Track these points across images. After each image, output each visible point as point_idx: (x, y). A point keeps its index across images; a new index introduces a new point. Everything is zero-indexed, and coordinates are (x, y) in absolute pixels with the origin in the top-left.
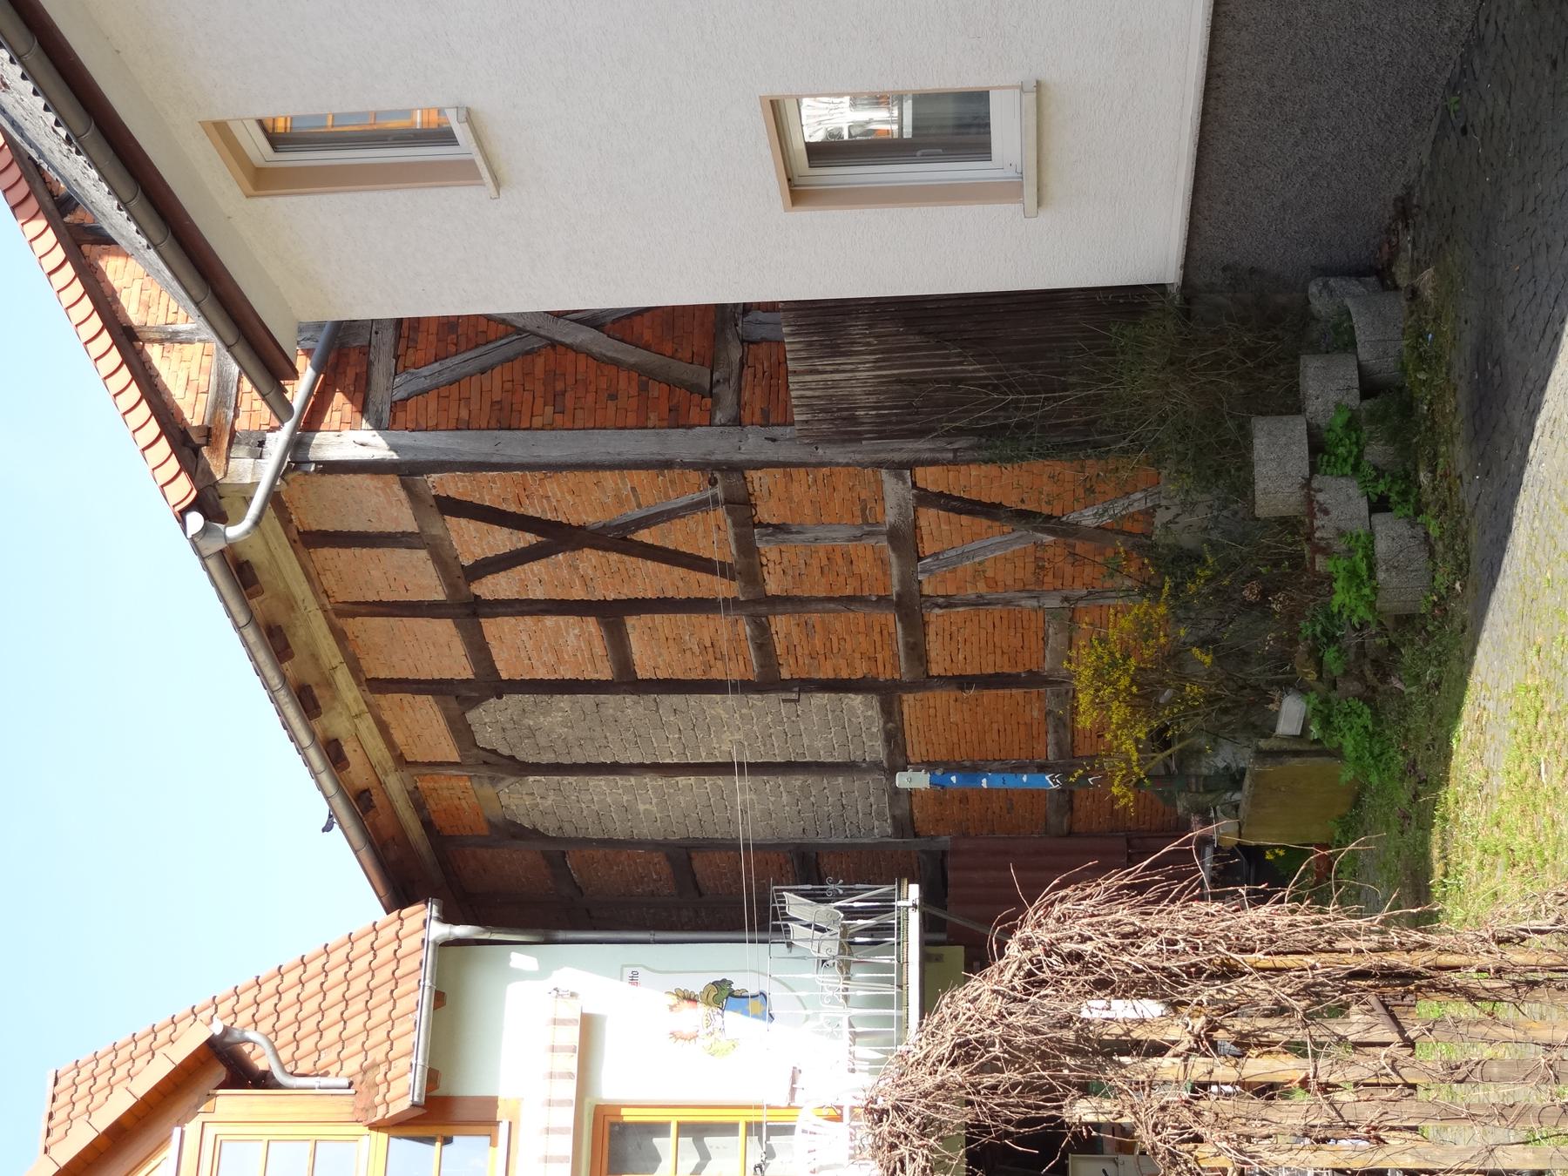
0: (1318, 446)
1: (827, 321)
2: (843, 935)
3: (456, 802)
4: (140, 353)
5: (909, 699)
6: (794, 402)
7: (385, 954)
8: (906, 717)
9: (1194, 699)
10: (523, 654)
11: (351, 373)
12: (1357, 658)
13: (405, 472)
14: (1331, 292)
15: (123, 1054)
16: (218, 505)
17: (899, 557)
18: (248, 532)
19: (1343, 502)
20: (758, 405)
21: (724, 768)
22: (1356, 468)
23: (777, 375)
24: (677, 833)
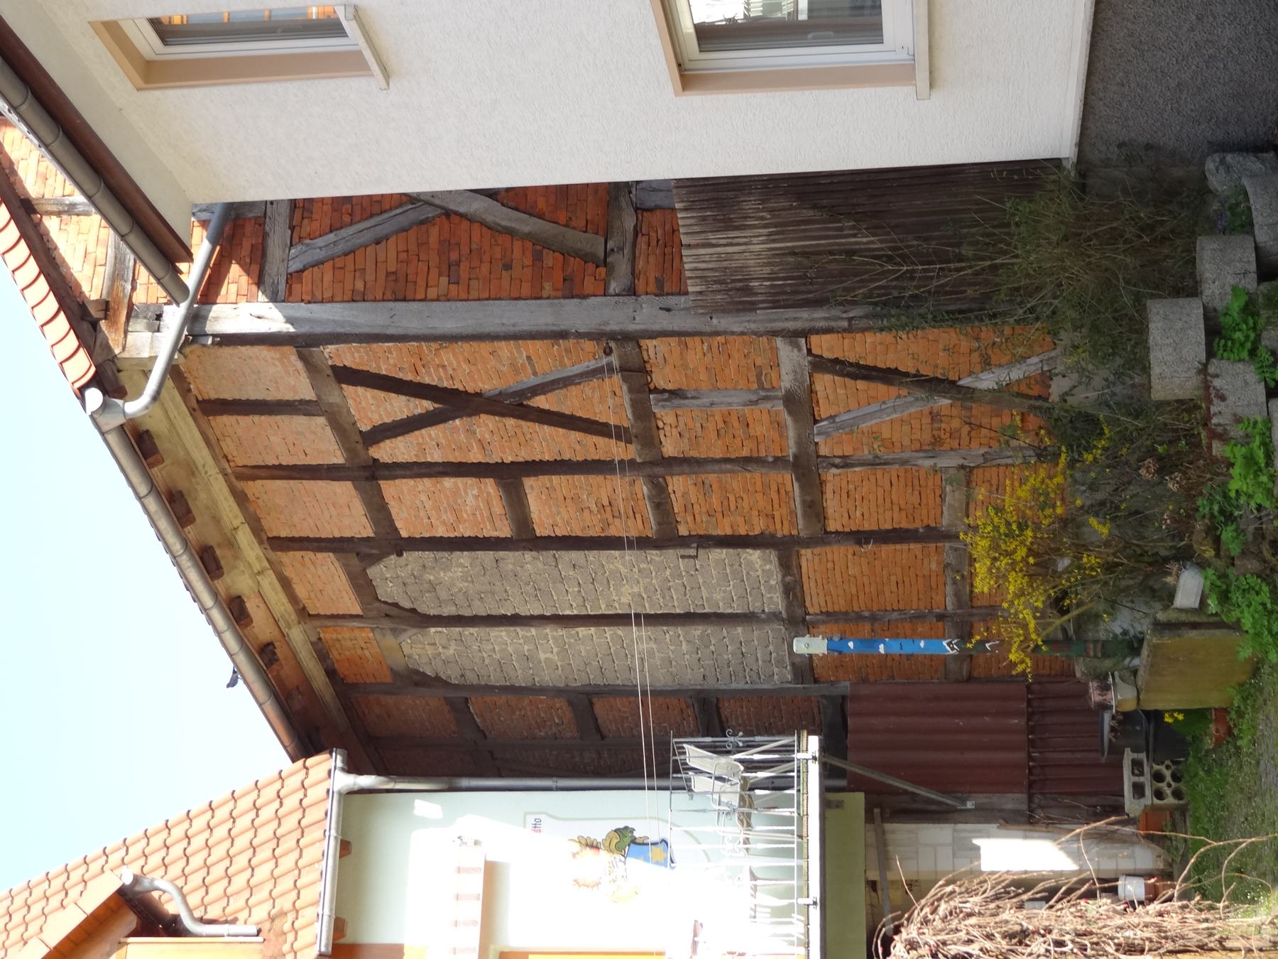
0: (1214, 331)
1: (720, 197)
2: (743, 788)
3: (359, 652)
4: (38, 226)
5: (806, 554)
6: (688, 274)
7: (291, 802)
8: (804, 570)
9: (1092, 569)
10: (422, 513)
11: (245, 251)
12: (1255, 538)
13: (302, 344)
14: (1228, 168)
15: (38, 892)
16: (117, 379)
17: (796, 420)
18: (146, 408)
19: (1241, 388)
20: (652, 275)
21: (621, 619)
22: (1253, 353)
23: (670, 246)
24: (578, 680)
